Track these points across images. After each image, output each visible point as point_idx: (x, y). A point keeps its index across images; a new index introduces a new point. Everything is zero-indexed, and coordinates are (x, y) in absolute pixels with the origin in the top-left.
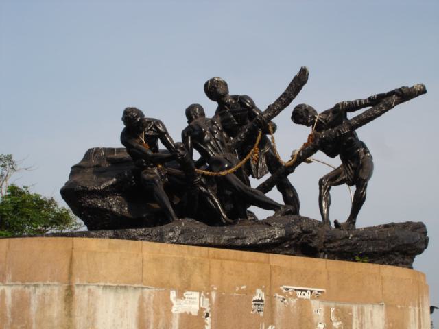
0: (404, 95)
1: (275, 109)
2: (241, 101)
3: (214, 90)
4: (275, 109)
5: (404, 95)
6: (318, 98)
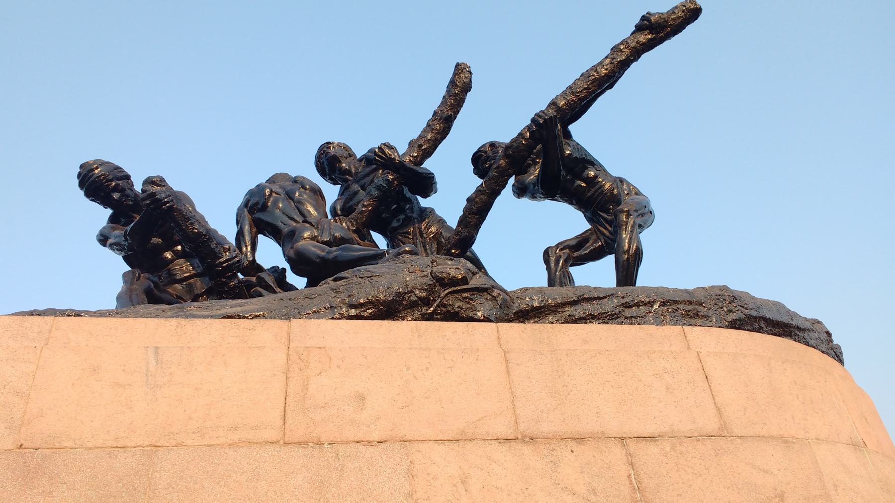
0: (656, 31)
1: (427, 145)
2: (380, 159)
3: (330, 162)
4: (427, 145)
5: (656, 31)
6: (498, 117)
